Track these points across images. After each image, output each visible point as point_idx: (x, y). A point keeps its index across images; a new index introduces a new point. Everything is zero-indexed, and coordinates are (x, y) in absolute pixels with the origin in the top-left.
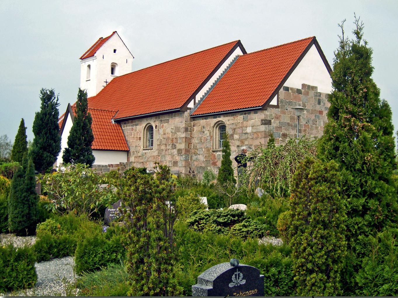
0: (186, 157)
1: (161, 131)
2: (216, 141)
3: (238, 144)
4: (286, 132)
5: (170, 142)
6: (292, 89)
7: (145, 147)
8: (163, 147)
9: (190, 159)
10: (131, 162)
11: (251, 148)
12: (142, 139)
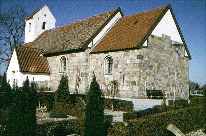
0: (86, 78)
1: (71, 61)
2: (105, 68)
3: (121, 71)
4: (152, 64)
5: (76, 68)
6: (156, 37)
7: (61, 71)
8: (72, 71)
9: (88, 79)
10: (52, 80)
11: (129, 74)
12: (59, 66)
